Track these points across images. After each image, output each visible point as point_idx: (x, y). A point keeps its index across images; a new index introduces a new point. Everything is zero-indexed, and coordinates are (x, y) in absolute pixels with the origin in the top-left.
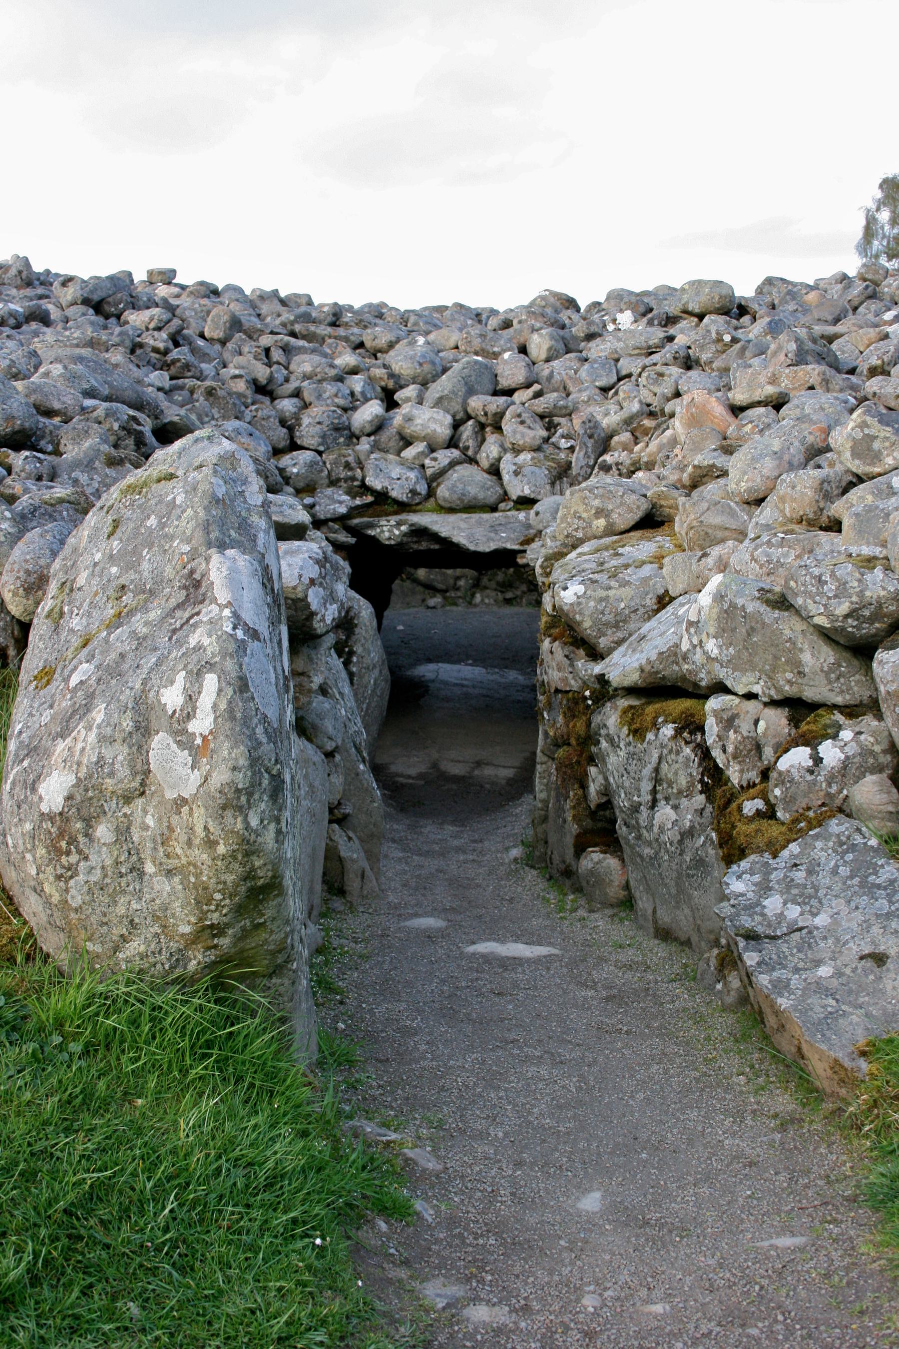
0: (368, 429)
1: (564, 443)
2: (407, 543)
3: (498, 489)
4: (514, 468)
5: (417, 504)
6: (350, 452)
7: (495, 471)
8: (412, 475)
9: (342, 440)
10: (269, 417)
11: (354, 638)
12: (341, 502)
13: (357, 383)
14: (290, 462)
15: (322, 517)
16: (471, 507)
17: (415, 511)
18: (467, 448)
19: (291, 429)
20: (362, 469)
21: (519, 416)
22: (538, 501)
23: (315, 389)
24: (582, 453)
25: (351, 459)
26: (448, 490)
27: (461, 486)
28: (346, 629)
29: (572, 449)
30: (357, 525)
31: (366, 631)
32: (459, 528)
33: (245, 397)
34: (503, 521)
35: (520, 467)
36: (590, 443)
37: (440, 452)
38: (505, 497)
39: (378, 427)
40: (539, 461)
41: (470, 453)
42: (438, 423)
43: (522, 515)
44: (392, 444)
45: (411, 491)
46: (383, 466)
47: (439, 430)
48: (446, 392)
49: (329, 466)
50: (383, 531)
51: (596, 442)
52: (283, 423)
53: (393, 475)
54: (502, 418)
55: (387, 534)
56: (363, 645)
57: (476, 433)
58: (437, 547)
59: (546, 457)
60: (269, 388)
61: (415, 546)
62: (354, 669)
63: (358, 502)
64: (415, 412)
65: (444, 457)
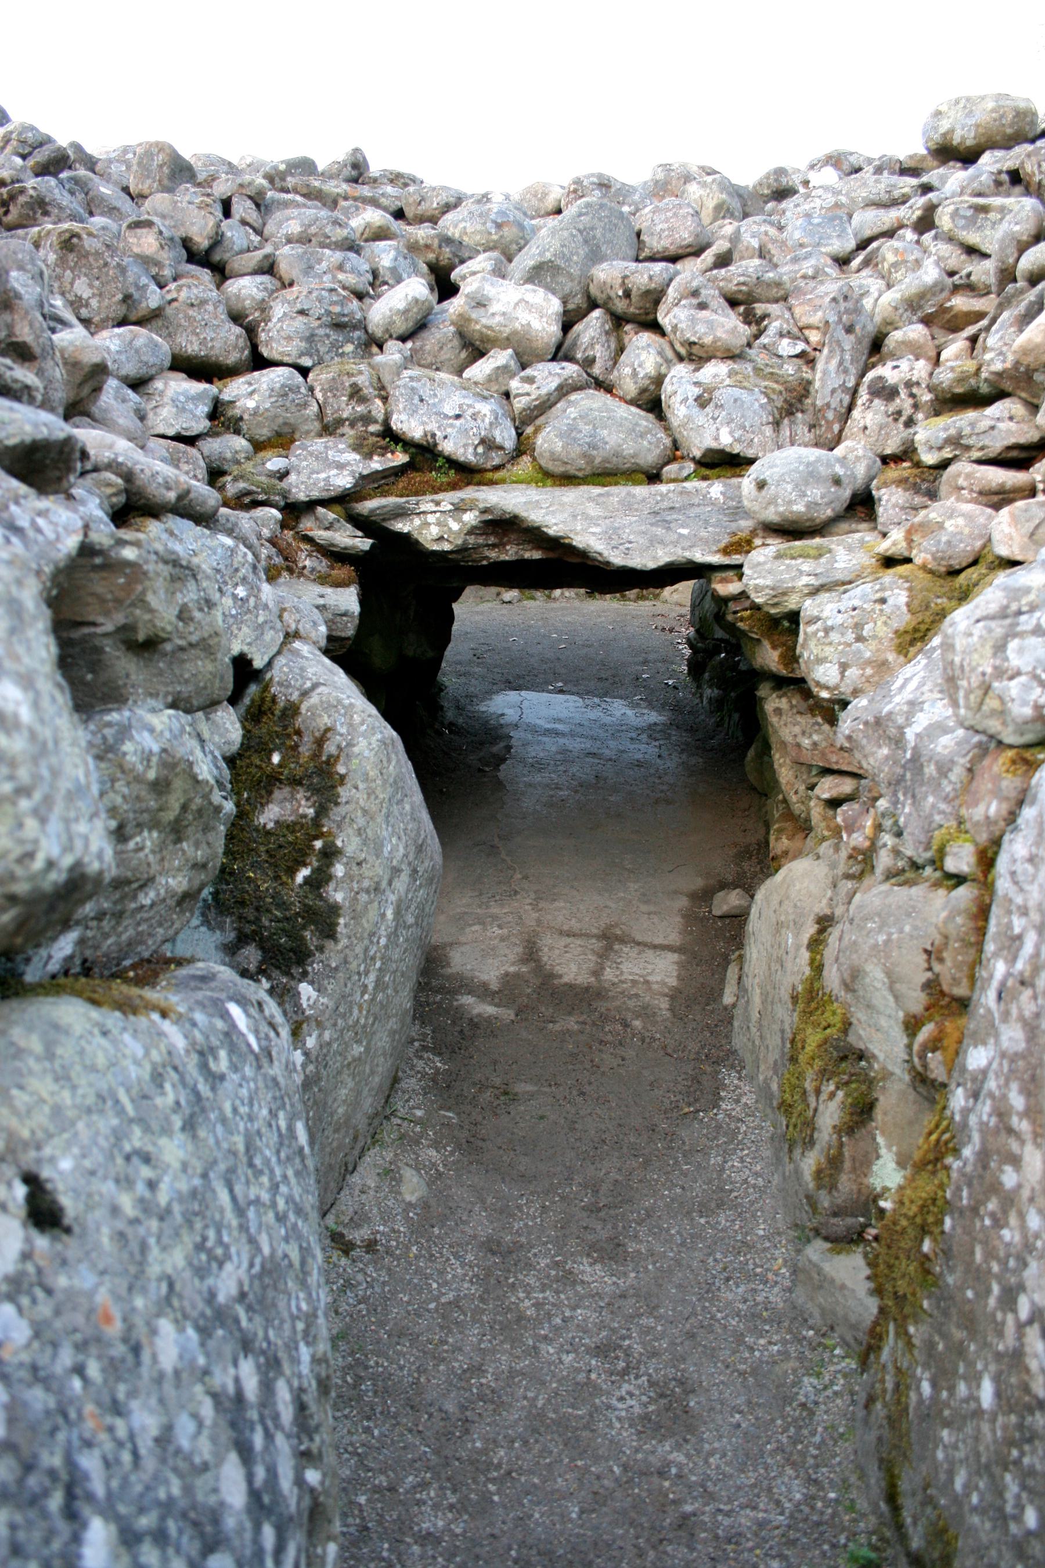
0: (401, 326)
1: (786, 348)
2: (477, 548)
3: (661, 435)
4: (697, 391)
5: (497, 468)
6: (362, 367)
7: (653, 404)
8: (486, 408)
9: (349, 348)
10: (203, 302)
11: (336, 813)
12: (341, 466)
13: (385, 254)
14: (246, 389)
15: (302, 497)
16: (606, 474)
17: (491, 483)
18: (589, 362)
19: (251, 331)
20: (385, 399)
21: (695, 293)
22: (751, 461)
23: (300, 257)
24: (834, 363)
25: (362, 380)
26: (560, 436)
27: (586, 429)
28: (316, 790)
29: (807, 359)
30: (372, 511)
31: (371, 793)
32: (586, 517)
33: (158, 264)
34: (678, 501)
35: (710, 390)
36: (848, 342)
37: (540, 366)
38: (675, 452)
39: (418, 328)
40: (746, 377)
41: (597, 370)
42: (536, 312)
43: (716, 489)
44: (447, 354)
45: (483, 441)
46: (426, 392)
47: (537, 325)
48: (548, 256)
49: (319, 395)
50: (427, 524)
51: (859, 341)
52: (236, 318)
53: (449, 411)
54: (657, 302)
55: (435, 531)
56: (359, 832)
57: (607, 333)
58: (537, 555)
59: (757, 370)
60: (216, 257)
61: (493, 555)
62: (339, 897)
63: (376, 464)
64: (490, 290)
65: (548, 376)
